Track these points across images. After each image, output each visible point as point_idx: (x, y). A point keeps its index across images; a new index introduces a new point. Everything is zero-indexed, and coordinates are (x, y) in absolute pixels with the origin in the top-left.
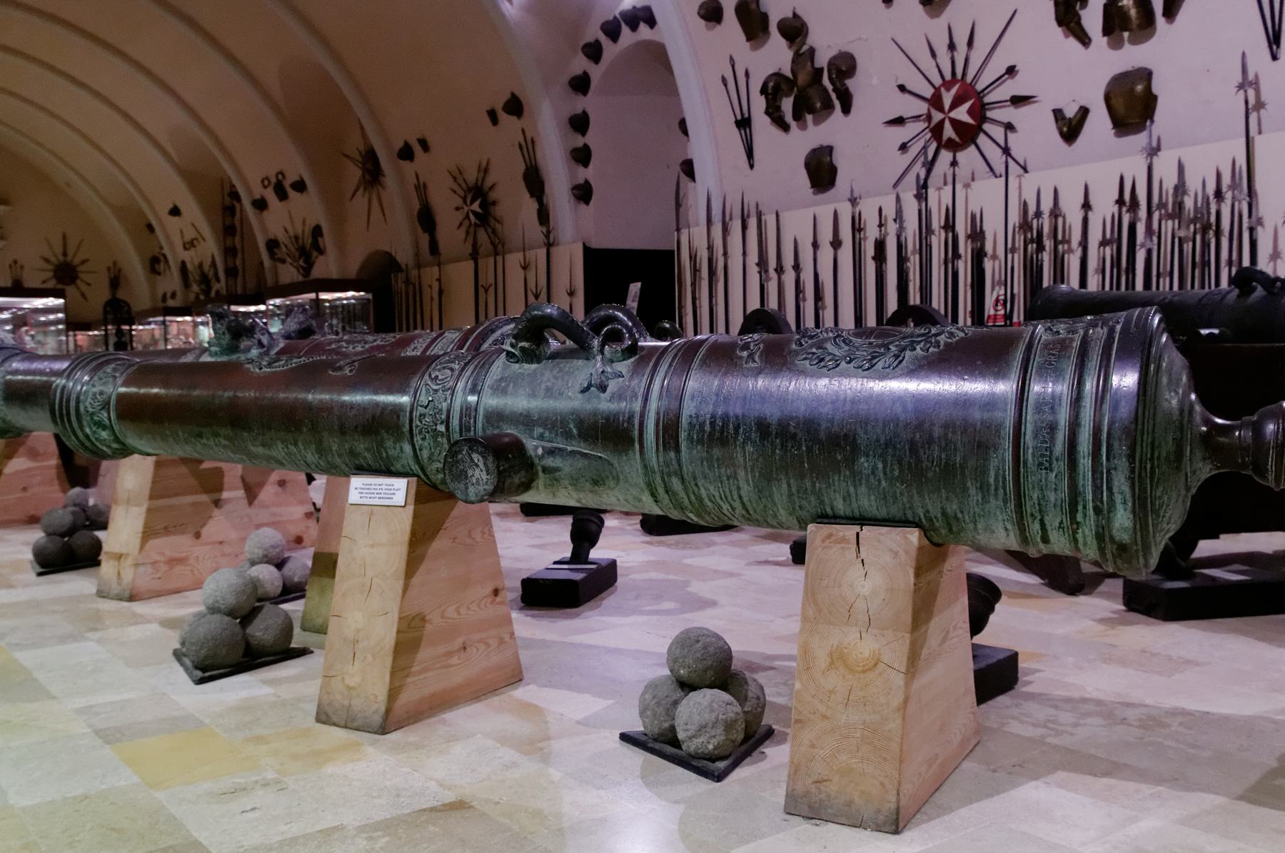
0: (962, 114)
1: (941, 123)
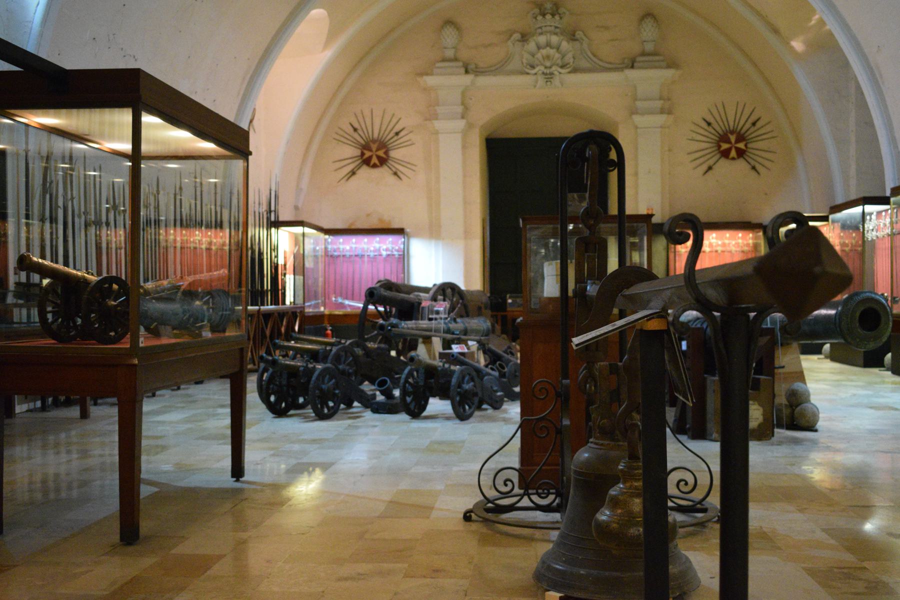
0: (381, 153)
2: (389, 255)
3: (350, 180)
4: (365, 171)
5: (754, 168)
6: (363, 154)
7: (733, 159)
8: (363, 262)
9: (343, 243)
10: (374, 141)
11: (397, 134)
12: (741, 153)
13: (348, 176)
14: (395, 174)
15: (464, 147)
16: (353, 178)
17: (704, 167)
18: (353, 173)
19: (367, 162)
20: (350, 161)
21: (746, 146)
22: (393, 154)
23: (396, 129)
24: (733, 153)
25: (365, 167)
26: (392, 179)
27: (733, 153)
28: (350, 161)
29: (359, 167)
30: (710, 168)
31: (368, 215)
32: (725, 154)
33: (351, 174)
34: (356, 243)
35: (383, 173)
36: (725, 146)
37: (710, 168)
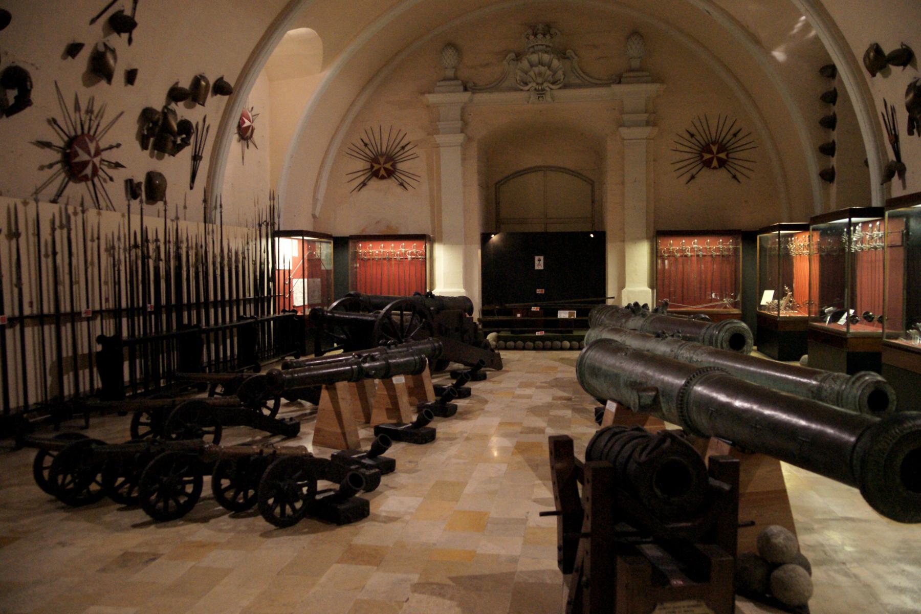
0: (388, 166)
1: (379, 170)
2: (414, 258)
3: (362, 190)
4: (374, 183)
5: (734, 177)
6: (372, 167)
7: (715, 168)
8: (391, 265)
9: (372, 248)
10: (382, 155)
11: (403, 148)
12: (722, 163)
13: (360, 186)
14: (401, 184)
15: (464, 160)
16: (364, 189)
17: (688, 176)
18: (364, 184)
19: (375, 174)
20: (361, 173)
21: (727, 155)
22: (400, 166)
23: (403, 143)
24: (715, 163)
25: (374, 178)
26: (399, 190)
27: (715, 163)
28: (361, 173)
29: (369, 179)
30: (693, 177)
31: (378, 222)
32: (707, 164)
33: (362, 185)
34: (384, 247)
35: (390, 184)
36: (707, 156)
37: (693, 177)
